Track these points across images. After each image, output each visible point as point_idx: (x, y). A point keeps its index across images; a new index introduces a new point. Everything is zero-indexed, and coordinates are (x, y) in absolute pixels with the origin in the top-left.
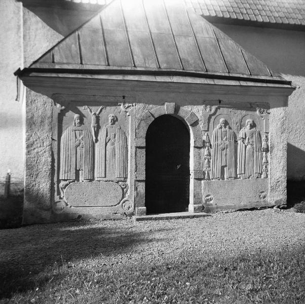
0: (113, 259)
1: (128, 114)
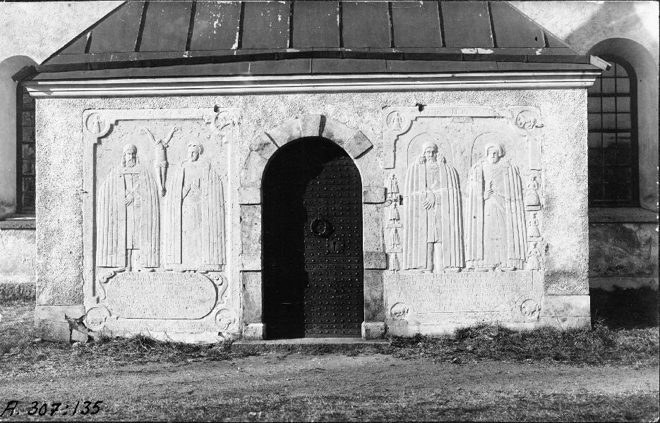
1: (224, 140)
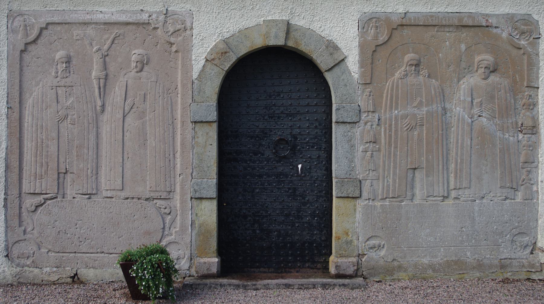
0: (217, 280)
1: (174, 48)
